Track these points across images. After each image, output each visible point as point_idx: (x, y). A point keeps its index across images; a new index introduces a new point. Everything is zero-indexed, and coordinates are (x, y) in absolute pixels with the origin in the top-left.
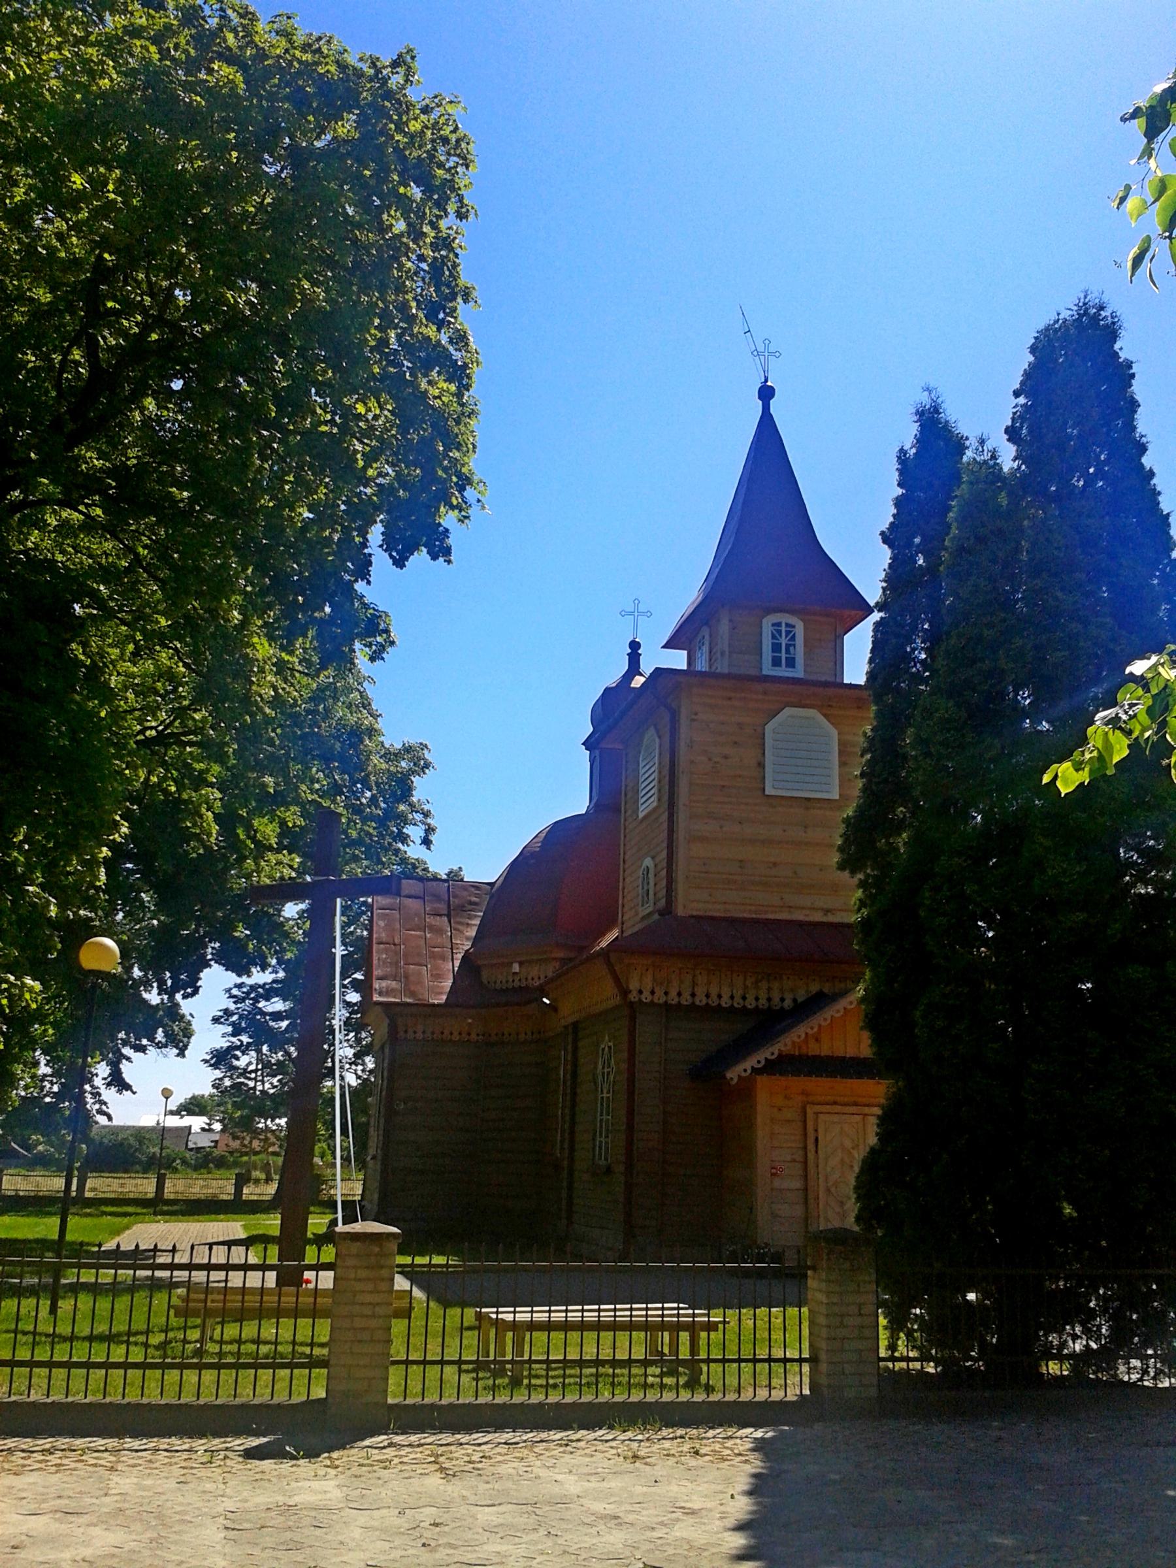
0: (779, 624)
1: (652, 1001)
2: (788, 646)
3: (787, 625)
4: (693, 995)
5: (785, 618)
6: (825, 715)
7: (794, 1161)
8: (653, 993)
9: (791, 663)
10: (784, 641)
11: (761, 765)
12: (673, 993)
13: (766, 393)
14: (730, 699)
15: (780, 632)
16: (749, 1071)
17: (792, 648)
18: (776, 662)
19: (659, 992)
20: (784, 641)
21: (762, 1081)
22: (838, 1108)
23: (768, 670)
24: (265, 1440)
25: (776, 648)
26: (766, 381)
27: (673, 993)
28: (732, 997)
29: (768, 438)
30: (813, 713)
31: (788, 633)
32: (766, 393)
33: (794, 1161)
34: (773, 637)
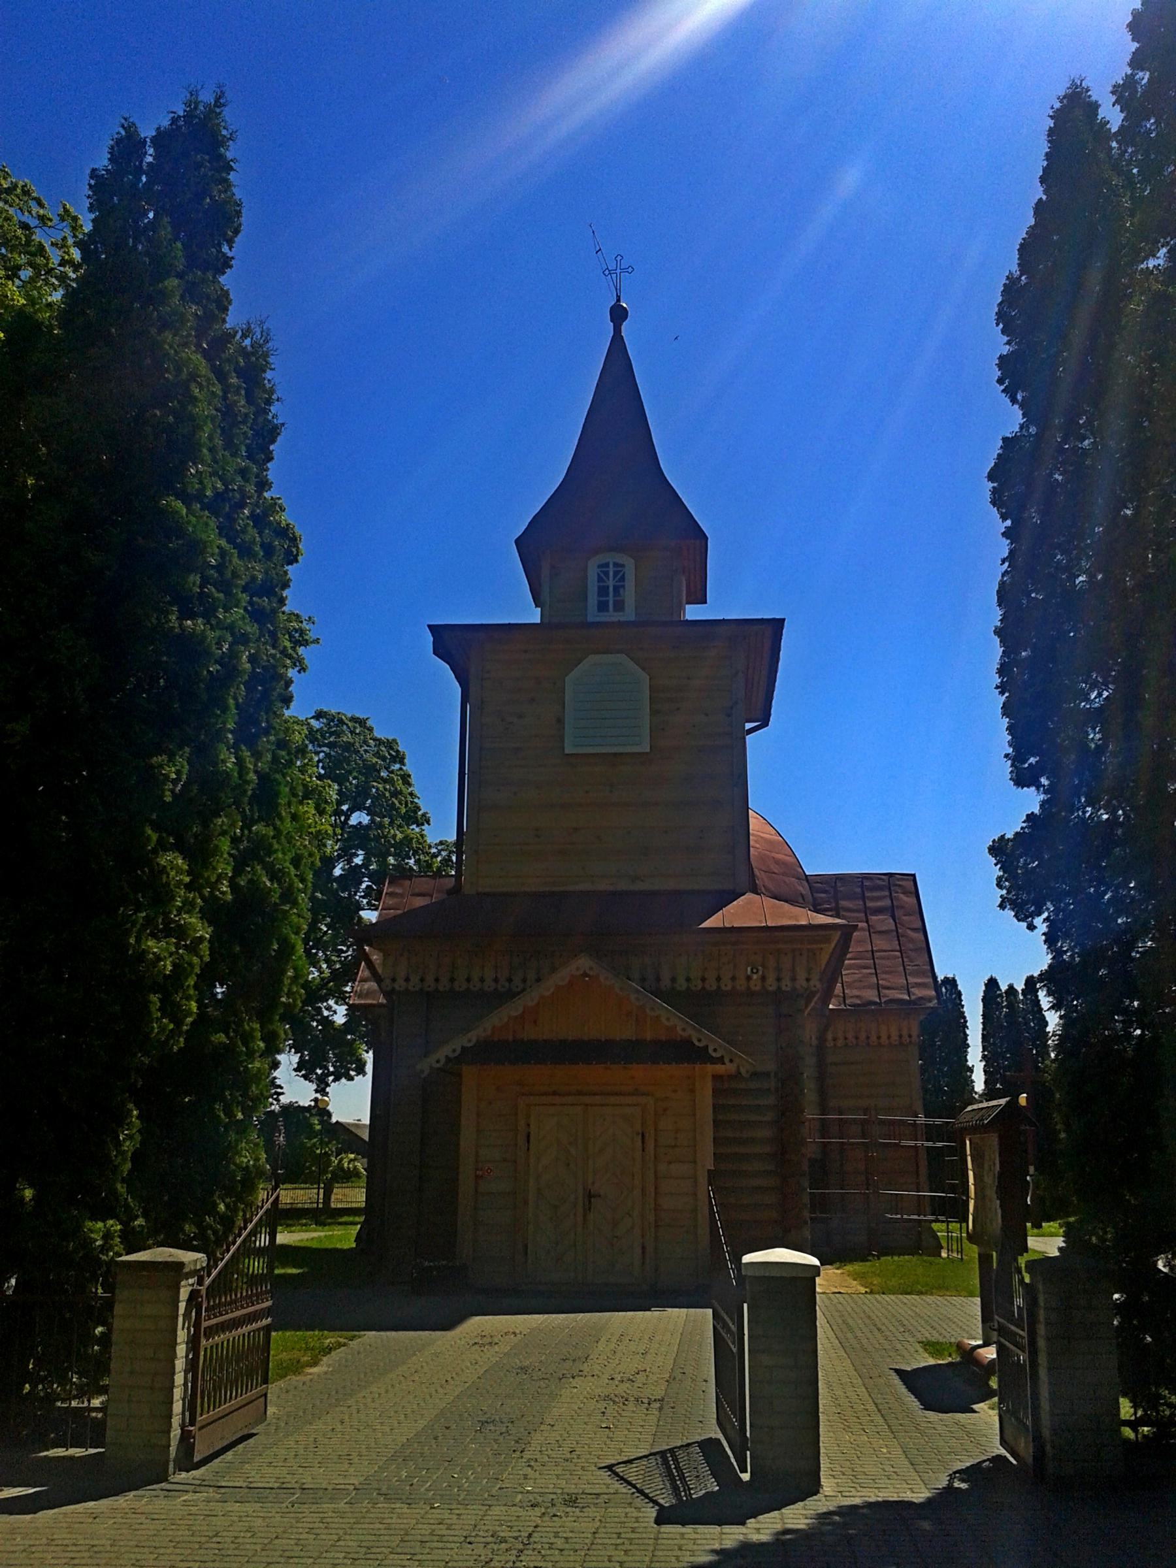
0: (607, 565)
1: (407, 989)
2: (616, 589)
3: (616, 565)
4: (452, 980)
5: (611, 558)
6: (636, 662)
7: (505, 1160)
8: (407, 980)
9: (619, 606)
10: (611, 583)
11: (560, 721)
12: (430, 979)
13: (618, 315)
14: (526, 652)
15: (607, 574)
16: (701, 1045)
17: (621, 590)
18: (602, 607)
19: (415, 980)
20: (611, 583)
21: (469, 1073)
22: (557, 1100)
23: (593, 615)
24: (32, 1491)
25: (603, 591)
26: (618, 300)
27: (430, 979)
28: (496, 980)
29: (618, 370)
30: (622, 658)
31: (616, 573)
32: (618, 315)
33: (505, 1160)
34: (600, 579)
